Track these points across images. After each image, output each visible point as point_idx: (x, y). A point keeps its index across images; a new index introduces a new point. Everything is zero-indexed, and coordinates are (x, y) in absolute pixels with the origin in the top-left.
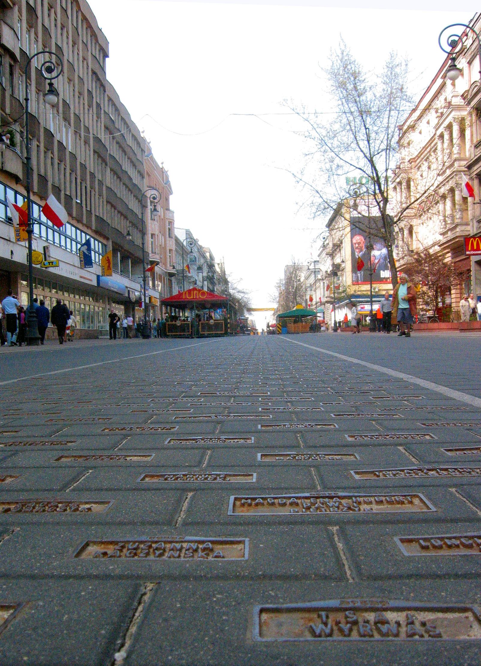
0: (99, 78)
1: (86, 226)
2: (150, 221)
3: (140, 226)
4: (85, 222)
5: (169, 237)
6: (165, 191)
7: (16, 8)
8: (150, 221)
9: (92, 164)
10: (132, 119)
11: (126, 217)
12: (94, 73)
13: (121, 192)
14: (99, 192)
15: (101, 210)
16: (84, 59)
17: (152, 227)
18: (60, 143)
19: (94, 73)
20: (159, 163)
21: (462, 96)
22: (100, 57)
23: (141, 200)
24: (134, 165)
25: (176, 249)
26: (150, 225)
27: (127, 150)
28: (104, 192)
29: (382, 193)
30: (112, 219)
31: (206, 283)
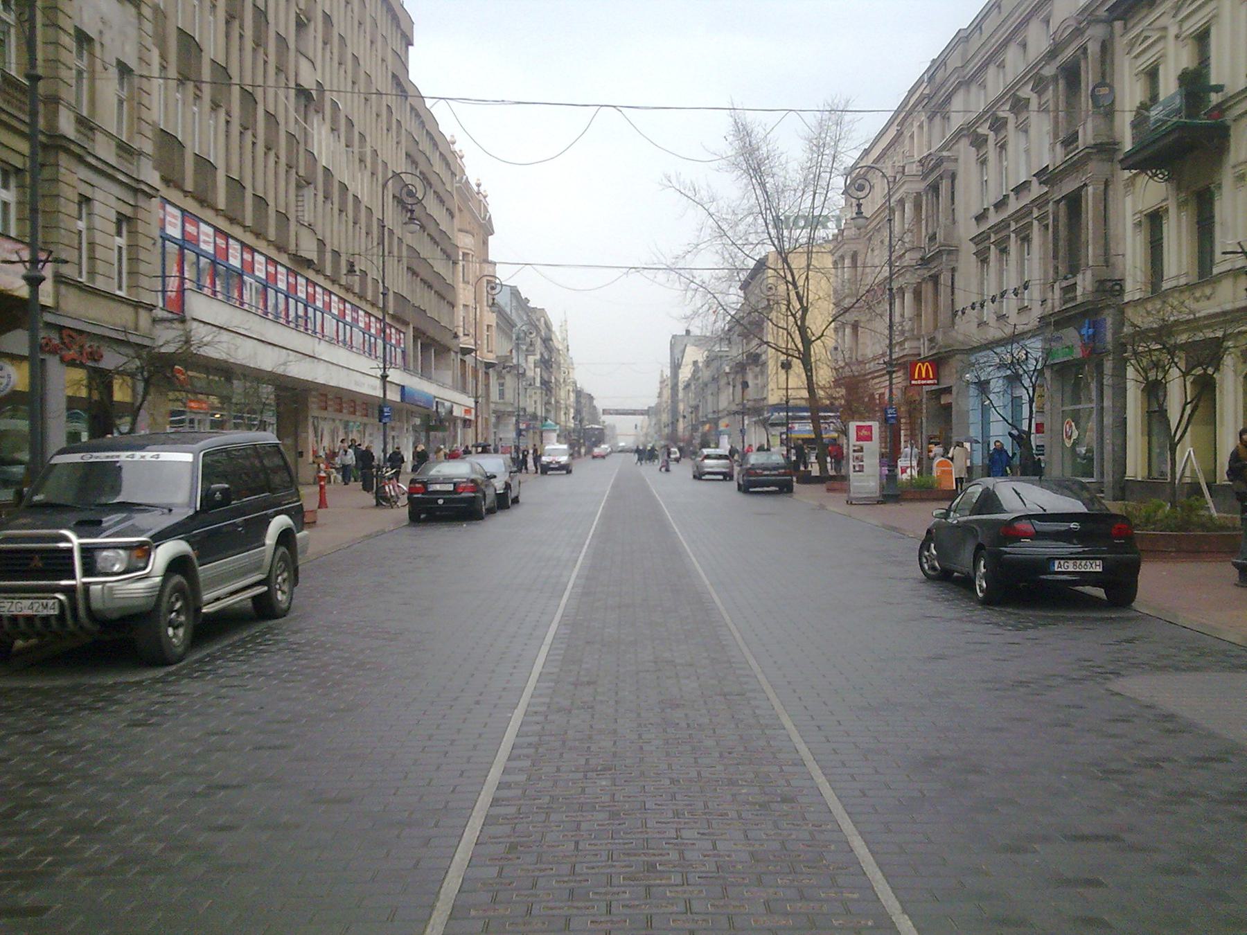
0: (401, 86)
1: (193, 197)
2: (461, 285)
3: (446, 296)
4: (189, 186)
5: (464, 281)
6: (485, 229)
7: (312, 25)
8: (461, 285)
9: (392, 217)
10: (411, 77)
11: (430, 287)
12: (394, 76)
13: (426, 250)
14: (266, 141)
15: (399, 282)
16: (383, 60)
17: (464, 295)
18: (355, 197)
19: (394, 76)
20: (473, 183)
21: (920, 161)
22: (396, 43)
23: (450, 257)
24: (442, 202)
25: (497, 324)
26: (461, 291)
27: (433, 179)
28: (404, 253)
29: (800, 299)
30: (413, 291)
31: (538, 370)
